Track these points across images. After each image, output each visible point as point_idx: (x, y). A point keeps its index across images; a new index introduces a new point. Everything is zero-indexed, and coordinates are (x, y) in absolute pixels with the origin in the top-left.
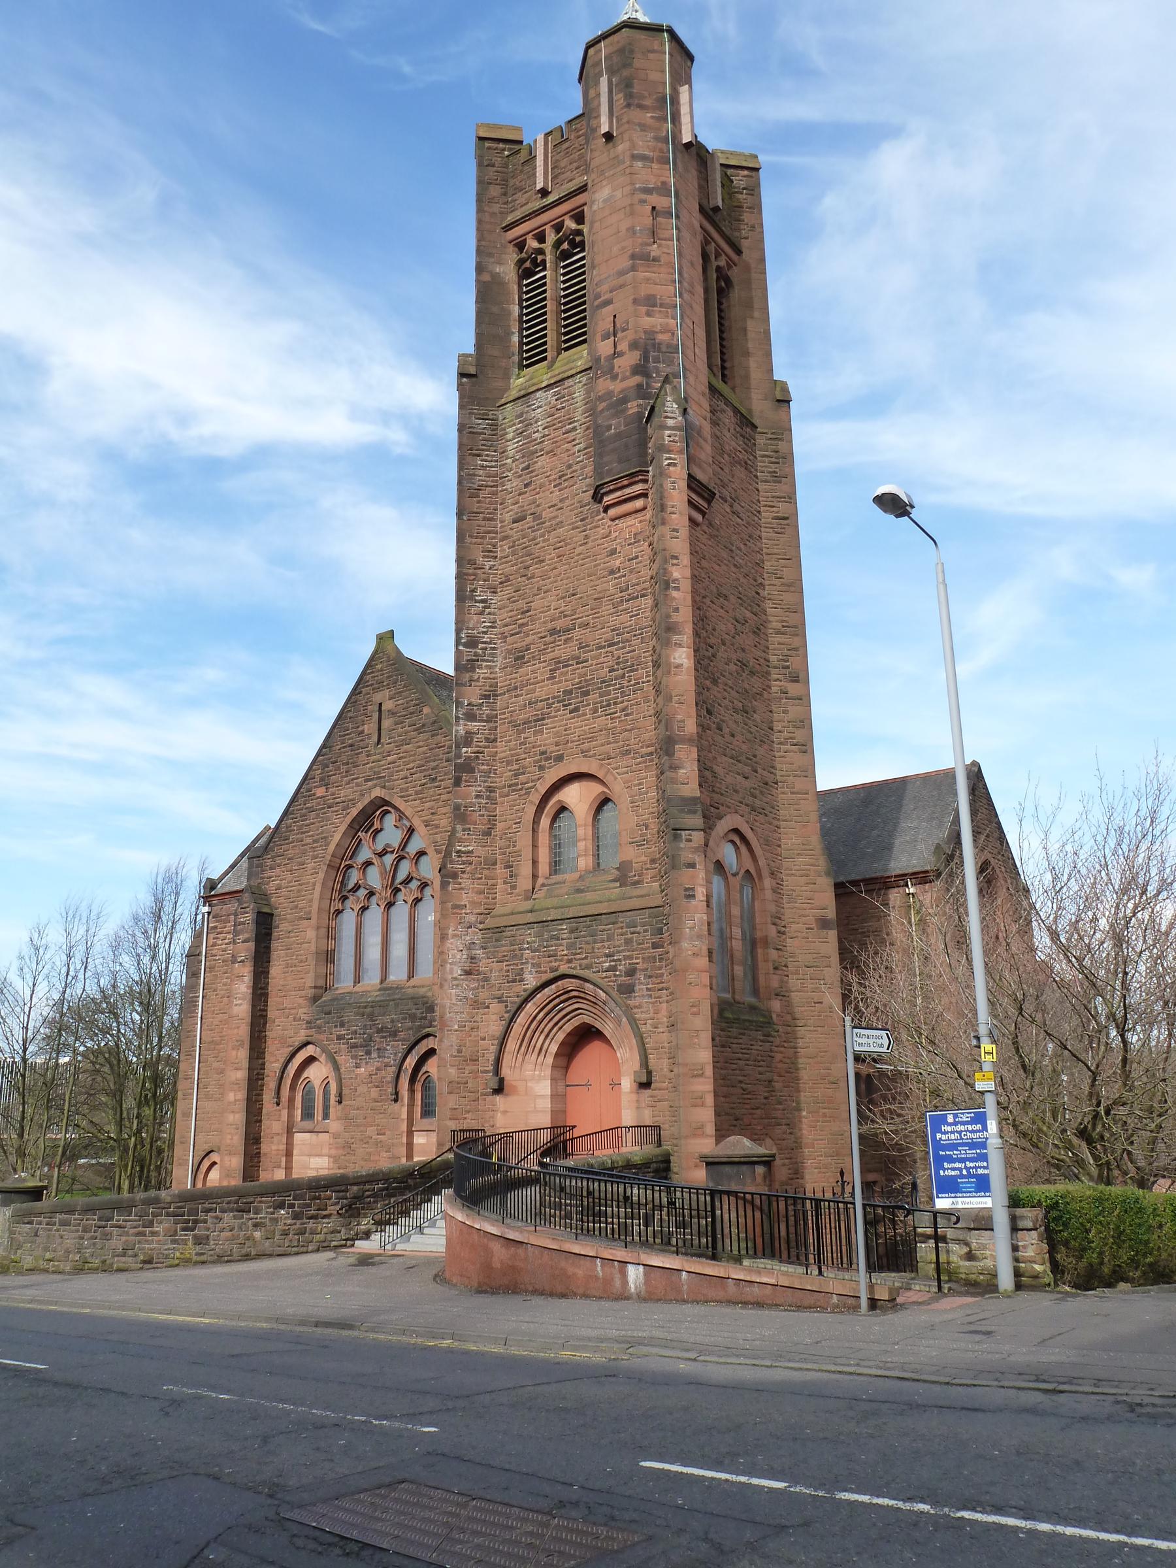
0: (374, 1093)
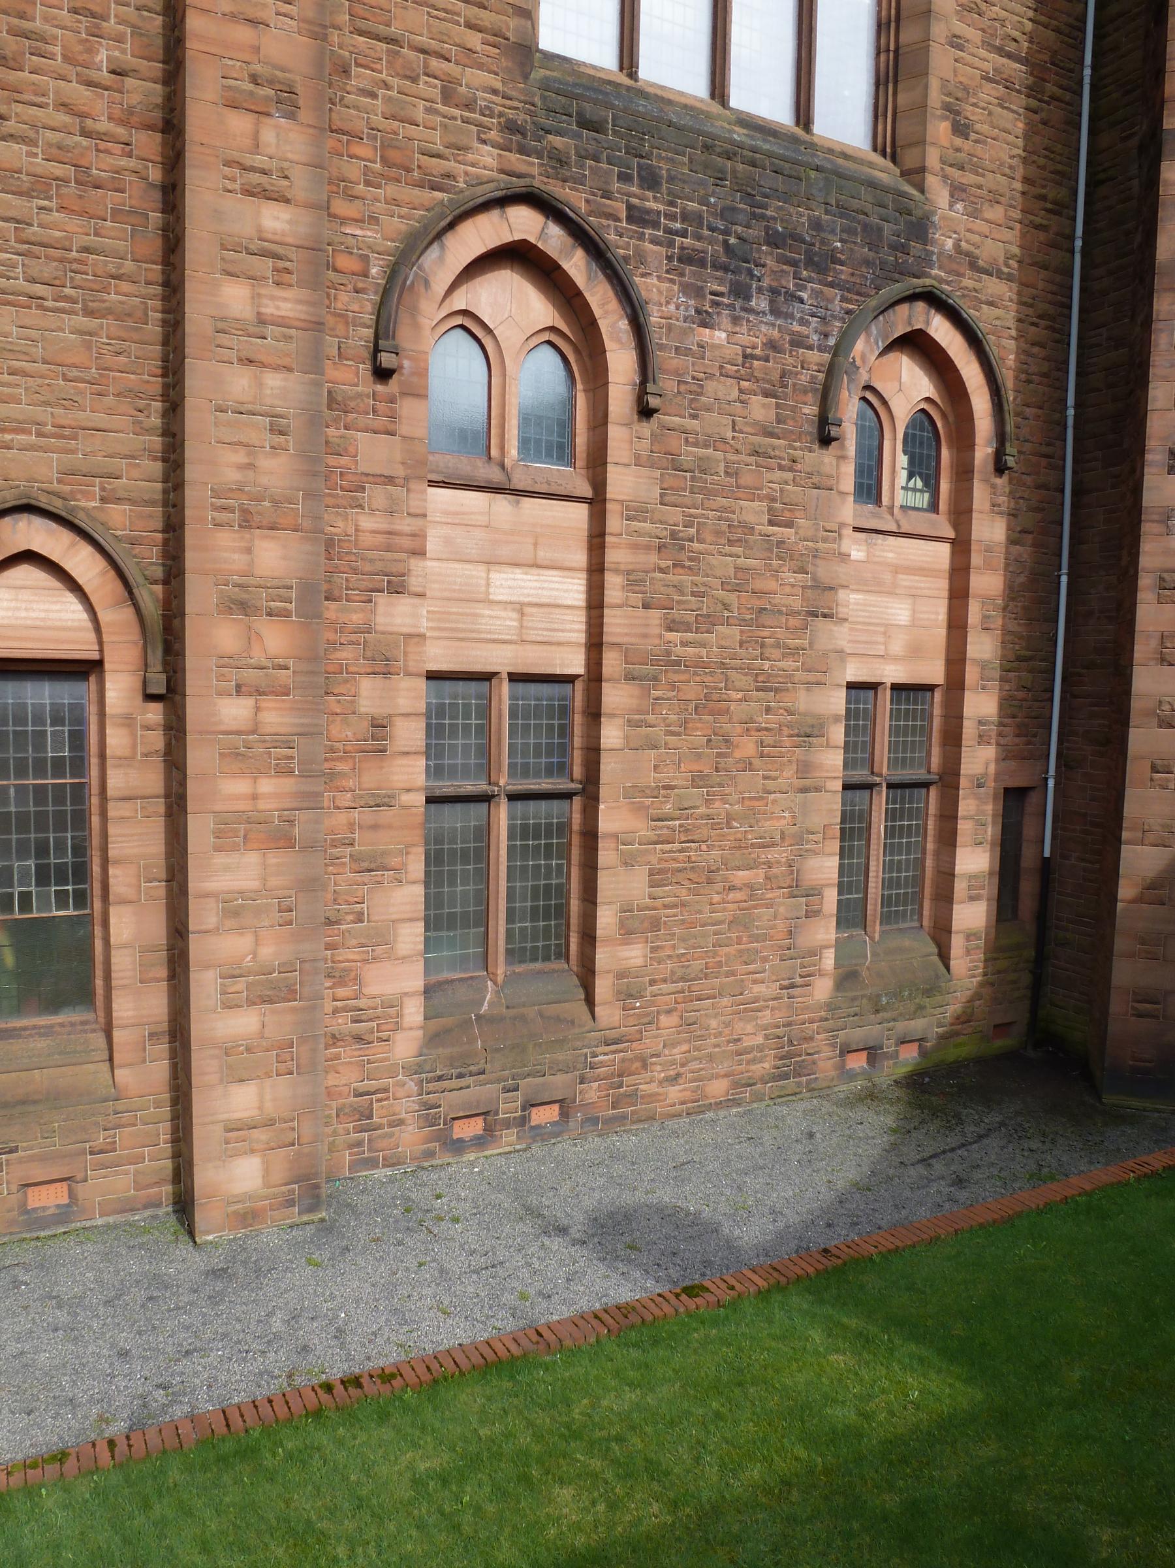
0: (760, 409)
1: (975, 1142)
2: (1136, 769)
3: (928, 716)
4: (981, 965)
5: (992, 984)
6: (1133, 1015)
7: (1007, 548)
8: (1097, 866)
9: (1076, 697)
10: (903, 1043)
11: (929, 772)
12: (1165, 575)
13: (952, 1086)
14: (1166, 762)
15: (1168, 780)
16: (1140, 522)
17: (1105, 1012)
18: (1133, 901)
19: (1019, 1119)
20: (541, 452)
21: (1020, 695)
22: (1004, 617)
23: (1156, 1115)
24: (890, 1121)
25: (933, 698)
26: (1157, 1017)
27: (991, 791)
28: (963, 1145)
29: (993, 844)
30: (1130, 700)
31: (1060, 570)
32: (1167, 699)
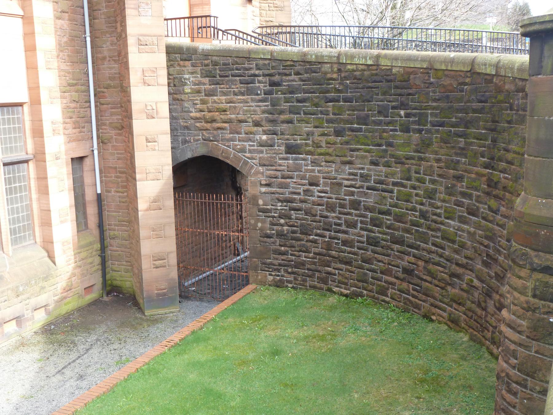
1: (85, 353)
2: (139, 142)
3: (21, 121)
4: (73, 257)
5: (80, 267)
6: (154, 268)
7: (55, 21)
8: (125, 194)
9: (103, 104)
10: (35, 310)
11: (27, 154)
12: (141, 38)
13: (67, 327)
14: (153, 137)
15: (155, 146)
16: (124, 9)
17: (140, 270)
18: (147, 210)
19: (106, 335)
20: (9, 113)
21: (73, 105)
22: (58, 61)
23: (171, 315)
24: (37, 355)
25: (23, 110)
26: (165, 266)
27: (64, 161)
28: (79, 357)
29: (69, 190)
30: (131, 105)
31: (85, 34)
32: (149, 103)
